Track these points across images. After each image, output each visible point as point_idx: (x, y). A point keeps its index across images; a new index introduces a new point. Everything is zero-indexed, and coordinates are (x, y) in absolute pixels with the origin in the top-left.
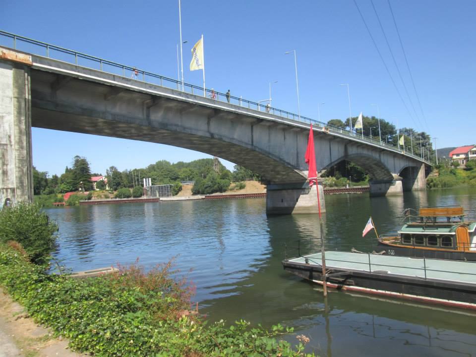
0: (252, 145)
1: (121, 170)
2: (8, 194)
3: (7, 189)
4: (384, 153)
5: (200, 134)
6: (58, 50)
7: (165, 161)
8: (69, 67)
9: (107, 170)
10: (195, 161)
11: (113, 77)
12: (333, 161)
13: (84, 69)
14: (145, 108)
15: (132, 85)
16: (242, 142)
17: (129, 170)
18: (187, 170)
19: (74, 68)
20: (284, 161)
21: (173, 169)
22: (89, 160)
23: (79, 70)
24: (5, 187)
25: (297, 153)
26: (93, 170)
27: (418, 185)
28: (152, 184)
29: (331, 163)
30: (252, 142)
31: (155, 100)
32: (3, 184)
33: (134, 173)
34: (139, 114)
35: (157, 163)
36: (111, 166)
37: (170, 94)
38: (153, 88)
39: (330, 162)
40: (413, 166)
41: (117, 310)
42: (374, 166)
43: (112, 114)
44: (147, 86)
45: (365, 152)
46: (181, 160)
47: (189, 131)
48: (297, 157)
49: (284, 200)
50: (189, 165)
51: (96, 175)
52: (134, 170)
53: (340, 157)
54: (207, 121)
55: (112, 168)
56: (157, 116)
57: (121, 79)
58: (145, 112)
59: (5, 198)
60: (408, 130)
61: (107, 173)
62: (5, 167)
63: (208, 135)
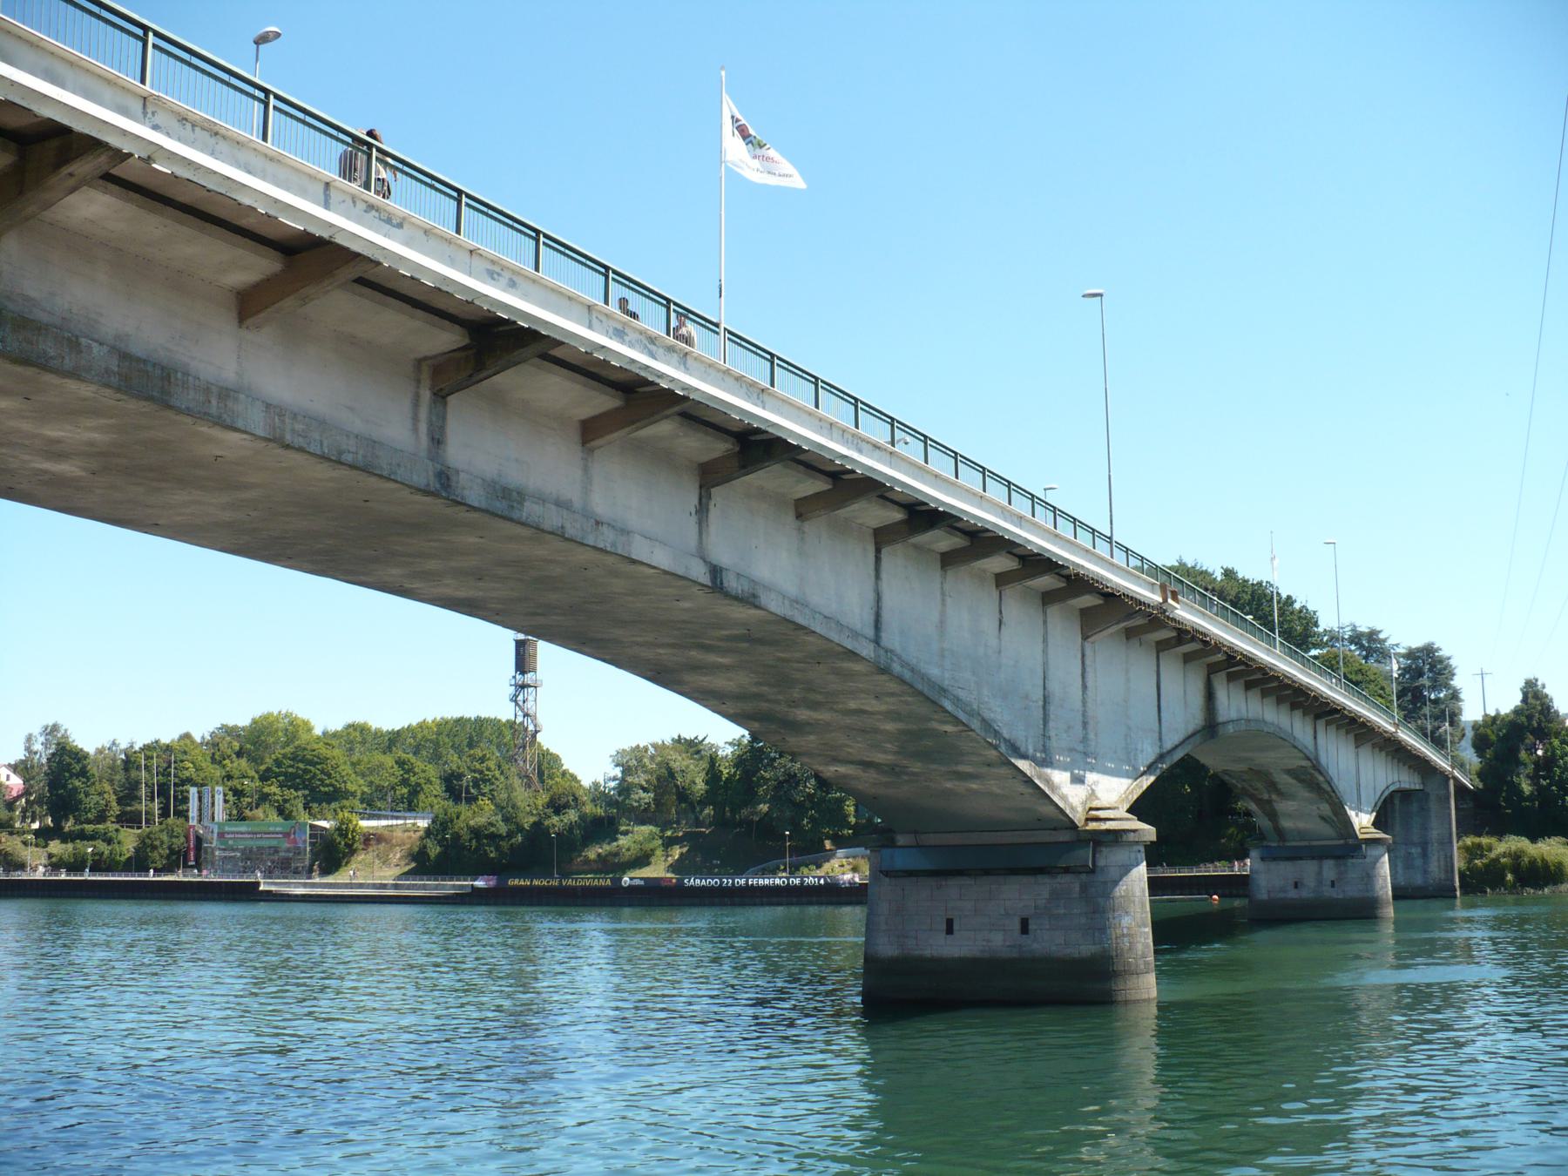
0: (877, 641)
1: (88, 739)
4: (1328, 724)
5: (661, 558)
9: (29, 739)
10: (422, 726)
11: (321, 188)
12: (1168, 745)
13: (183, 119)
14: (426, 395)
15: (407, 244)
17: (124, 746)
19: (137, 106)
20: (997, 734)
21: (324, 751)
23: (159, 118)
27: (1425, 872)
29: (1161, 757)
31: (490, 344)
33: (148, 758)
34: (388, 420)
35: (254, 721)
37: (579, 322)
38: (504, 281)
39: (1157, 751)
40: (1406, 786)
41: (1511, 949)
42: (1284, 780)
43: (268, 406)
44: (476, 261)
46: (359, 718)
47: (606, 539)
49: (956, 927)
50: (393, 740)
52: (146, 748)
53: (1191, 729)
54: (694, 500)
56: (492, 447)
58: (423, 413)
60: (1362, 634)
61: (28, 749)
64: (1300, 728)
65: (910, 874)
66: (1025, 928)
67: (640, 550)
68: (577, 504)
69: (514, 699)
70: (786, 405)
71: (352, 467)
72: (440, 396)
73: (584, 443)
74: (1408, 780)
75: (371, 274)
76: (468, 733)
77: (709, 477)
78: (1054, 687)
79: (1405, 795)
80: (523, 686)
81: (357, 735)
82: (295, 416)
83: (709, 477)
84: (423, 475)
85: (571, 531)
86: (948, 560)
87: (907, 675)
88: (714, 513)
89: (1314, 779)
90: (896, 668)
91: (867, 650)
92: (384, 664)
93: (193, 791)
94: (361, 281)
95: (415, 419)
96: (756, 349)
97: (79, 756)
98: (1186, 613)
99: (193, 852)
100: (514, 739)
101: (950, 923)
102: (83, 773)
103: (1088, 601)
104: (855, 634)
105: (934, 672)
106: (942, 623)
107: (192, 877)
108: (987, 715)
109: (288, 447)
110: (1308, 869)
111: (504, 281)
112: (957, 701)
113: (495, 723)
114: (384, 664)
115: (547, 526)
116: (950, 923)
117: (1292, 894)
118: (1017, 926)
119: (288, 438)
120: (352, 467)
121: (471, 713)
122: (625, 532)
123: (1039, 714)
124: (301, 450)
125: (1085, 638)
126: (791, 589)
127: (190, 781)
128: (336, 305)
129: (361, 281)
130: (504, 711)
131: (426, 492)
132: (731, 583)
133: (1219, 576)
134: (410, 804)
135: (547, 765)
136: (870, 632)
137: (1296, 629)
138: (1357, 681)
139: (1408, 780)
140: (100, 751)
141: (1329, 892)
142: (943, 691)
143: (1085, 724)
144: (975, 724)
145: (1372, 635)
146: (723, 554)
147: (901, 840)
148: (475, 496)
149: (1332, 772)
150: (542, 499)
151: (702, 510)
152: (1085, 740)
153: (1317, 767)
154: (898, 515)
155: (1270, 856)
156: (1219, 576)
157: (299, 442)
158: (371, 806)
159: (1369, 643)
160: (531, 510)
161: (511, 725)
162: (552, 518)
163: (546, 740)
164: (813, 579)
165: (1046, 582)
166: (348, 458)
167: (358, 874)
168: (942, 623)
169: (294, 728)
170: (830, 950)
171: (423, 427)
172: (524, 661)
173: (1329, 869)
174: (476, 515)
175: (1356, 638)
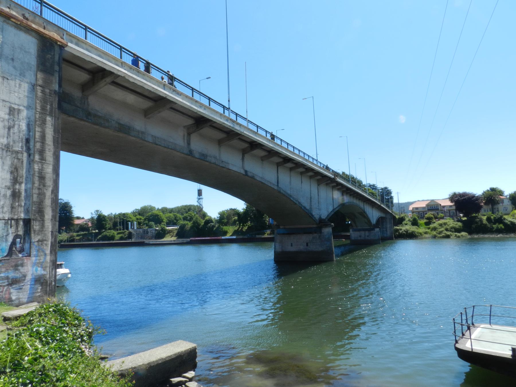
0: (278, 186)
1: (106, 212)
2: (19, 229)
3: (17, 221)
6: (98, 37)
7: (150, 206)
8: (113, 61)
16: (271, 183)
17: (114, 214)
18: (171, 215)
22: (72, 204)
24: (16, 217)
25: (311, 198)
26: (76, 212)
28: (138, 228)
29: (334, 209)
30: (278, 183)
31: (200, 122)
32: (12, 212)
36: (96, 209)
38: (203, 108)
45: (356, 201)
48: (311, 201)
50: (171, 211)
51: (78, 218)
55: (97, 211)
57: (172, 90)
58: (186, 138)
59: (14, 234)
62: (17, 187)
63: (243, 172)
64: (361, 204)
65: (283, 234)
66: (307, 245)
67: (231, 167)
68: (218, 158)
69: (198, 202)
70: (260, 136)
71: (171, 149)
72: (189, 134)
73: (219, 145)
74: (383, 215)
75: (174, 106)
76: (188, 209)
77: (244, 152)
78: (312, 195)
79: (382, 218)
80: (200, 199)
81: (164, 210)
82: (158, 138)
83: (244, 152)
84: (186, 151)
85: (217, 163)
86: (291, 169)
87: (284, 193)
88: (245, 160)
89: (363, 214)
90: (282, 191)
91: (276, 188)
92: (171, 193)
93: (130, 223)
94: (172, 108)
95: (184, 139)
96: (254, 124)
97: (104, 217)
98: (339, 180)
99: (130, 236)
100: (199, 210)
101: (292, 244)
102: (105, 220)
103: (319, 177)
104: (274, 185)
105: (289, 192)
106: (290, 182)
107: (130, 241)
108: (300, 201)
109: (157, 145)
110: (363, 233)
111: (203, 108)
112: (293, 198)
113: (194, 206)
114: (171, 193)
115: (212, 162)
116: (292, 244)
117: (359, 238)
118: (306, 244)
119: (157, 142)
120: (171, 149)
121: (188, 204)
122: (228, 163)
123: (309, 201)
124: (160, 145)
125: (318, 185)
126: (261, 176)
127: (129, 221)
128: (166, 113)
129: (172, 108)
130: (196, 204)
131: (187, 155)
132: (249, 174)
133: (341, 173)
134: (174, 224)
135: (204, 215)
136: (276, 184)
137: (359, 184)
138: (373, 195)
139: (383, 215)
140: (108, 215)
141: (367, 238)
142: (291, 196)
143: (319, 203)
144: (297, 203)
145: (374, 185)
146: (247, 168)
147: (281, 227)
148: (197, 155)
149: (368, 213)
150: (211, 157)
151: (243, 159)
152: (319, 206)
153: (364, 212)
154: (281, 160)
155: (355, 230)
156: (341, 173)
157: (159, 143)
158: (169, 224)
159: (373, 187)
160: (209, 159)
161: (197, 206)
162: (213, 160)
163: (204, 209)
164: (266, 174)
165: (311, 174)
166: (170, 147)
167: (168, 239)
168: (290, 182)
169: (152, 208)
170: (86, 330)
171: (186, 141)
172: (200, 193)
173: (367, 233)
174: (197, 160)
175: (370, 186)
